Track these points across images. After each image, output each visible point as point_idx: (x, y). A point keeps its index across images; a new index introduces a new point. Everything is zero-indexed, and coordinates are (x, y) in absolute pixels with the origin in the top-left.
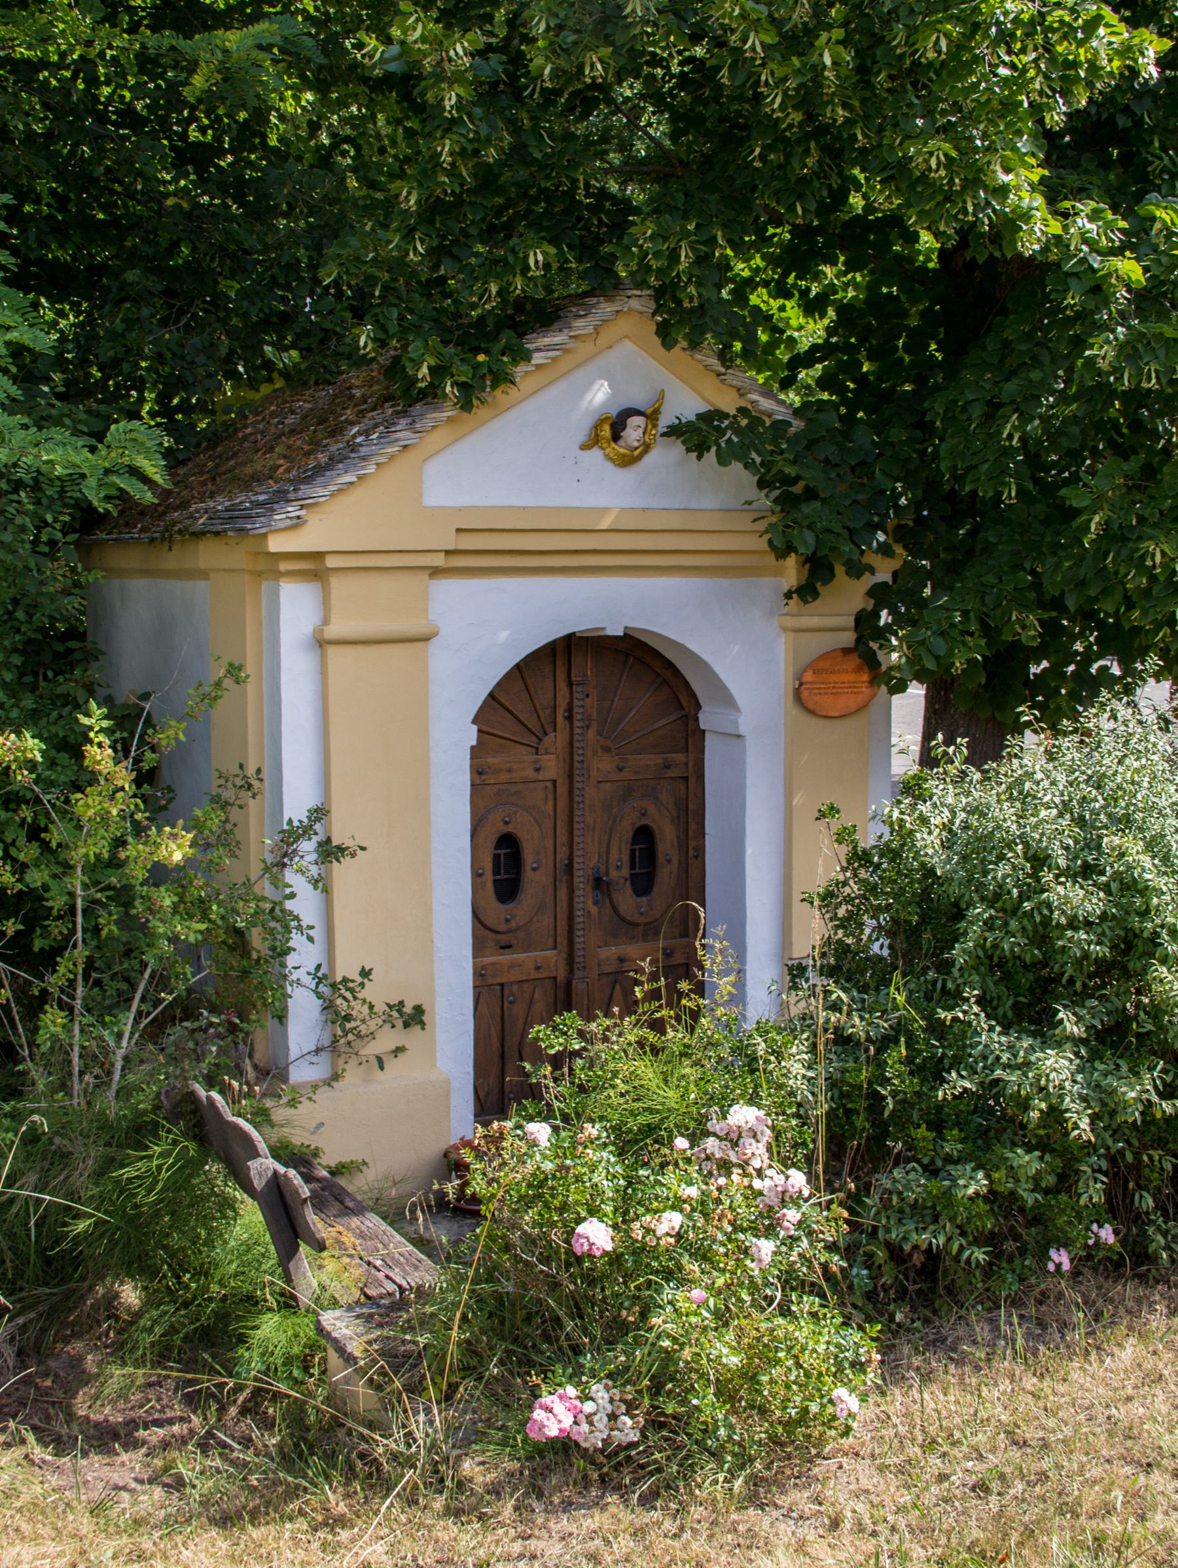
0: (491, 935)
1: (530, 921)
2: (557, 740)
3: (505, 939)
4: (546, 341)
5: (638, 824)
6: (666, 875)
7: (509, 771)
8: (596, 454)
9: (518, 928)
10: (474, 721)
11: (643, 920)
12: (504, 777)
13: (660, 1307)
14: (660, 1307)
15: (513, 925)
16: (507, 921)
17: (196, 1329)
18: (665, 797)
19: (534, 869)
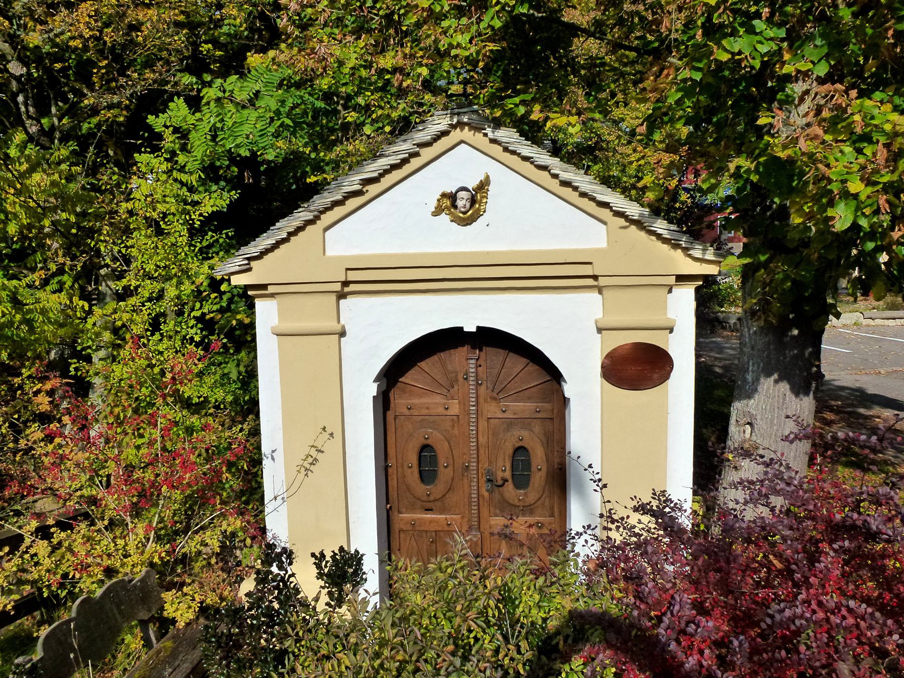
0: (419, 503)
1: (444, 495)
2: (32, 551)
3: (429, 505)
4: (395, 149)
5: (517, 445)
6: (538, 478)
7: (428, 408)
8: (445, 218)
9: (435, 500)
10: (478, 328)
11: (521, 503)
12: (425, 412)
13: (233, 490)
14: (233, 490)
15: (432, 498)
16: (428, 495)
17: (99, 125)
18: (537, 429)
19: (446, 467)
